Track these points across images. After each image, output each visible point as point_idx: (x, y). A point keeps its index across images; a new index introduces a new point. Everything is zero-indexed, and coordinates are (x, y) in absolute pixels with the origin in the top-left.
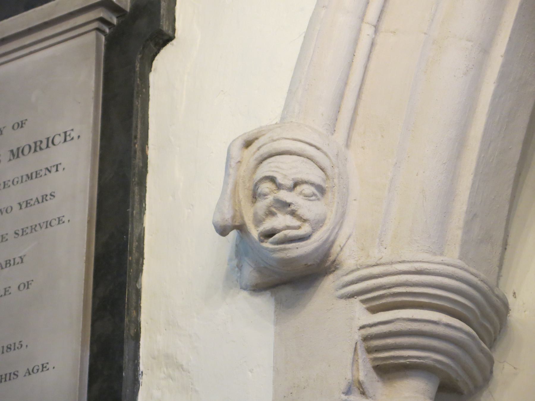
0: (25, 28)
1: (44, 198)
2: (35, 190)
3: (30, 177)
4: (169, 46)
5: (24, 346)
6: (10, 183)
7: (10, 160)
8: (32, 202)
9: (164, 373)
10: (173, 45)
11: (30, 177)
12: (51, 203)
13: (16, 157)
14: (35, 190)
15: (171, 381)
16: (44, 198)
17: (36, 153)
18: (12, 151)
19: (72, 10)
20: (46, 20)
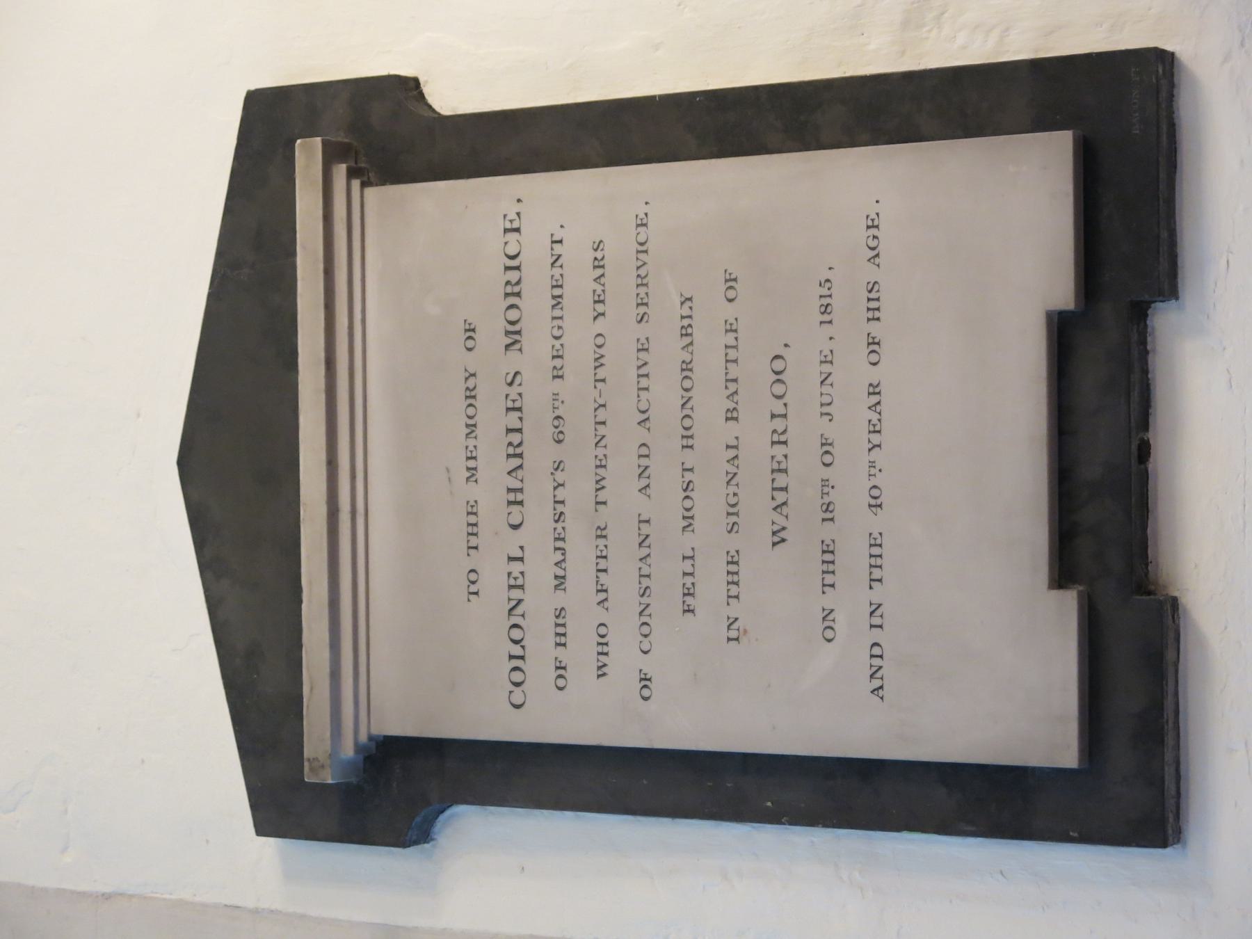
0: (323, 396)
1: (598, 264)
2: (579, 285)
3: (557, 300)
4: (426, 90)
5: (829, 275)
6: (557, 343)
7: (520, 350)
8: (599, 289)
9: (930, 31)
10: (426, 82)
11: (557, 300)
12: (609, 252)
13: (517, 337)
14: (579, 285)
15: (946, 15)
16: (598, 264)
17: (523, 294)
18: (507, 347)
19: (320, 213)
20: (321, 266)
